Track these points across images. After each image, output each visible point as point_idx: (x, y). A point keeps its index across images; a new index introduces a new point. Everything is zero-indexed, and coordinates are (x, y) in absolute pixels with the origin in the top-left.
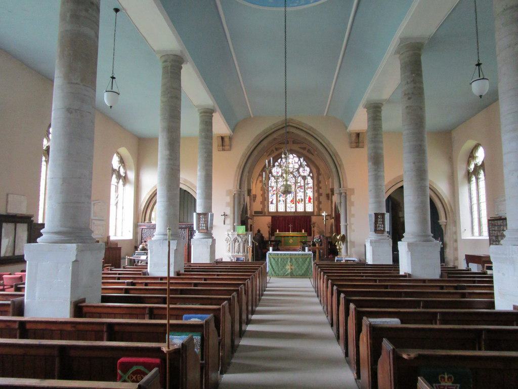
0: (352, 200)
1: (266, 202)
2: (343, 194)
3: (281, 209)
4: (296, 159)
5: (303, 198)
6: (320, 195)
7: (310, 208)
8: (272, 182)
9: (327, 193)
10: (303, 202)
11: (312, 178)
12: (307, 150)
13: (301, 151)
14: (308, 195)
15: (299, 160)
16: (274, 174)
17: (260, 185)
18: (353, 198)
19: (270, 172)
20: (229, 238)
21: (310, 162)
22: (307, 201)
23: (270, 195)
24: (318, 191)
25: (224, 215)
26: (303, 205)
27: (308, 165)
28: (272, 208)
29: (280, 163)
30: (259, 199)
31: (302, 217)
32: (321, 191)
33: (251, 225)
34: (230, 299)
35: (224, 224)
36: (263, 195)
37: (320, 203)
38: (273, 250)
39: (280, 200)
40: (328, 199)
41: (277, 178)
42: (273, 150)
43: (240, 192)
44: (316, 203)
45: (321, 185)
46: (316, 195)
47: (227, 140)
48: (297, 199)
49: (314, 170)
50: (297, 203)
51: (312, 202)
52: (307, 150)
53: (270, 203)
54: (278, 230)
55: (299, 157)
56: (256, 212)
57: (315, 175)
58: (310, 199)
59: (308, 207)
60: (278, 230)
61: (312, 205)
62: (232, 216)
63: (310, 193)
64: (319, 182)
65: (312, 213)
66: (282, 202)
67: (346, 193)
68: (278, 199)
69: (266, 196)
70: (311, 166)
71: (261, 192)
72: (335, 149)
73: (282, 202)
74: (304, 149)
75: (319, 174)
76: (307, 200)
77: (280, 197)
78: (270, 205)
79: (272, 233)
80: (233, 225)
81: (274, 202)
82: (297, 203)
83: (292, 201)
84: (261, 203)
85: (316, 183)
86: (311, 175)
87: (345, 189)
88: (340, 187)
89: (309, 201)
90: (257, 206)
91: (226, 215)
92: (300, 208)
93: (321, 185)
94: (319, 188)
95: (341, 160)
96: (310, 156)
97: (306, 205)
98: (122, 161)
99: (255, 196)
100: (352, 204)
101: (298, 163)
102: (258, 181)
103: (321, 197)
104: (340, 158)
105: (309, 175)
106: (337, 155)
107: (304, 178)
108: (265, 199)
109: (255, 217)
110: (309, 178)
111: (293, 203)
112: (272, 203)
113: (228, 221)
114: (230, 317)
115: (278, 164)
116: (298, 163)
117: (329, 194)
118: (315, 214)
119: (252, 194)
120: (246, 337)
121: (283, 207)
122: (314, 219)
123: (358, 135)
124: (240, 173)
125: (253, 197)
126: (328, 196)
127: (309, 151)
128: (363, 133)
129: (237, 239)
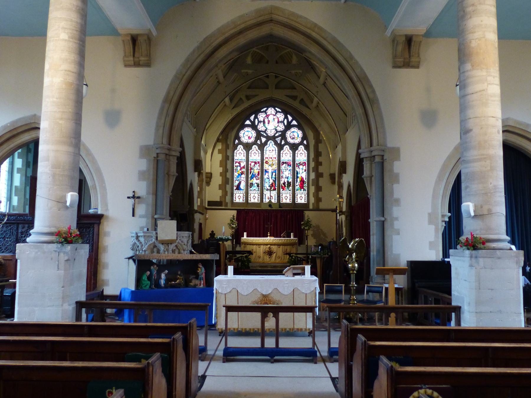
0: (396, 170)
1: (228, 187)
2: (377, 159)
3: (254, 198)
4: (281, 117)
5: (290, 180)
6: (319, 175)
7: (301, 198)
8: (240, 154)
9: (332, 172)
10: (291, 188)
11: (307, 147)
12: (298, 100)
13: (290, 101)
14: (299, 175)
15: (286, 117)
16: (245, 140)
17: (218, 157)
18: (398, 167)
19: (238, 138)
20: (138, 243)
21: (304, 122)
22: (297, 187)
23: (236, 174)
24: (316, 169)
25: (134, 197)
26: (291, 192)
27: (299, 127)
28: (239, 197)
29: (253, 122)
30: (217, 180)
31: (290, 211)
32: (321, 169)
33: (200, 225)
34: (186, 328)
35: (133, 216)
36: (223, 174)
37: (318, 189)
38: (236, 272)
39: (252, 184)
40: (333, 182)
41: (248, 147)
42: (241, 99)
43: (169, 150)
44: (312, 189)
45: (321, 159)
46: (313, 176)
47: (140, 40)
48: (282, 182)
49: (311, 135)
50: (281, 190)
51: (306, 188)
52: (298, 100)
53: (235, 188)
54: (245, 234)
55: (286, 113)
56: (210, 203)
57: (312, 143)
58: (302, 181)
59: (299, 196)
60: (245, 234)
61: (306, 192)
62: (150, 199)
63: (302, 173)
64: (318, 154)
65: (305, 206)
66: (255, 187)
67: (383, 156)
68: (250, 182)
69: (229, 167)
70: (306, 128)
71: (221, 170)
72: (362, 69)
73: (255, 187)
74: (294, 98)
75: (318, 140)
76: (298, 183)
77: (252, 178)
78: (235, 192)
79: (237, 236)
80: (153, 217)
81: (243, 186)
82: (281, 190)
83: (272, 186)
84: (220, 187)
85: (312, 156)
86: (305, 142)
87: (383, 148)
88: (371, 146)
89: (302, 187)
90: (213, 193)
91: (139, 198)
92: (286, 197)
93: (321, 159)
94: (318, 163)
95: (374, 91)
96: (305, 111)
97: (296, 192)
98: (355, 304)
99: (210, 176)
100: (396, 179)
101: (283, 122)
102: (216, 151)
103: (321, 179)
104: (371, 86)
105: (301, 143)
106: (364, 79)
107: (294, 147)
108: (227, 181)
109: (208, 211)
110: (301, 148)
111: (275, 189)
112: (238, 188)
113: (141, 209)
114: (164, 381)
115: (250, 123)
116: (283, 122)
117: (334, 174)
118: (311, 207)
119: (204, 172)
120: (214, 360)
121: (256, 195)
122: (308, 215)
123: (409, 40)
124: (171, 112)
125: (207, 177)
126: (332, 177)
127: (302, 102)
128: (417, 36)
129: (155, 246)
